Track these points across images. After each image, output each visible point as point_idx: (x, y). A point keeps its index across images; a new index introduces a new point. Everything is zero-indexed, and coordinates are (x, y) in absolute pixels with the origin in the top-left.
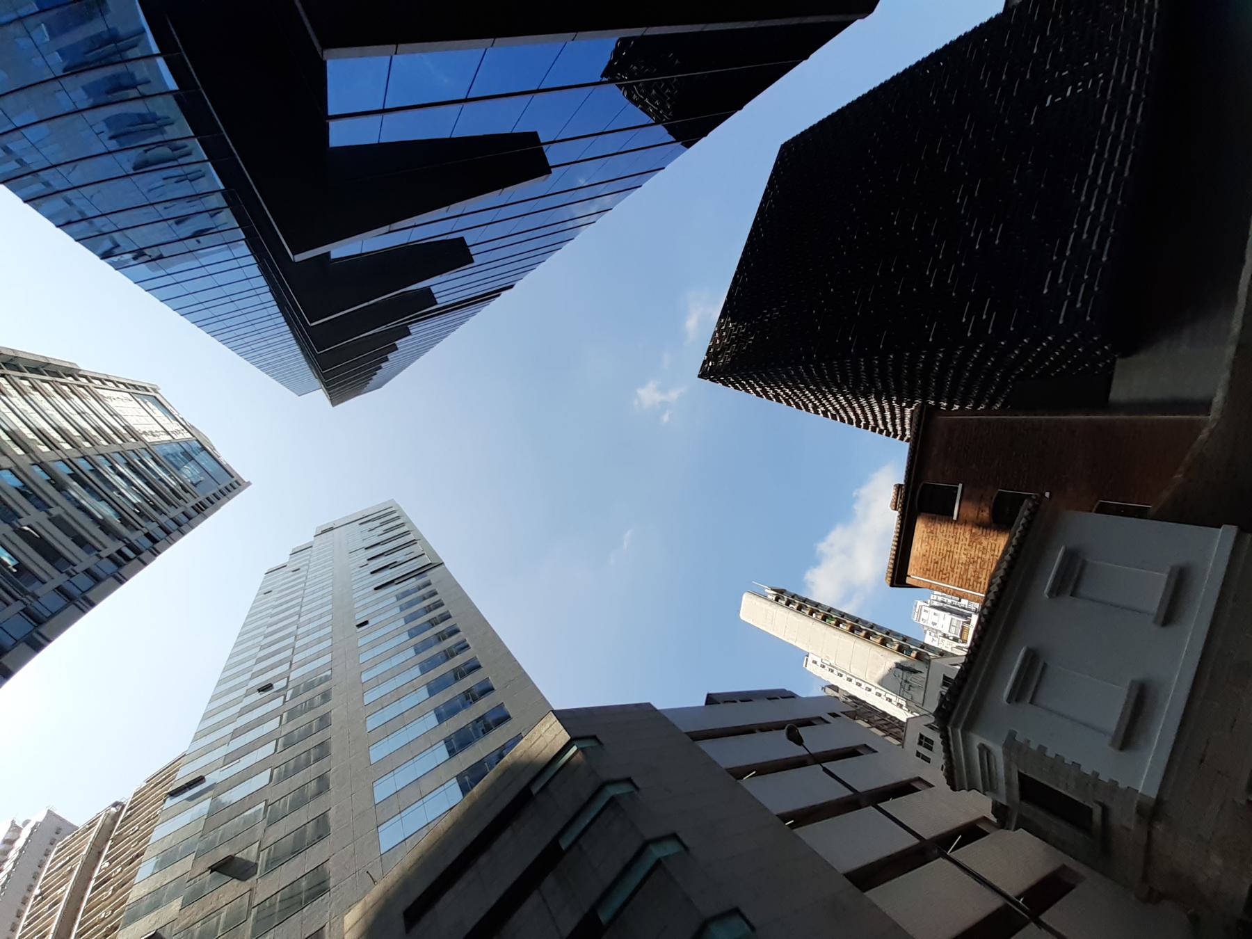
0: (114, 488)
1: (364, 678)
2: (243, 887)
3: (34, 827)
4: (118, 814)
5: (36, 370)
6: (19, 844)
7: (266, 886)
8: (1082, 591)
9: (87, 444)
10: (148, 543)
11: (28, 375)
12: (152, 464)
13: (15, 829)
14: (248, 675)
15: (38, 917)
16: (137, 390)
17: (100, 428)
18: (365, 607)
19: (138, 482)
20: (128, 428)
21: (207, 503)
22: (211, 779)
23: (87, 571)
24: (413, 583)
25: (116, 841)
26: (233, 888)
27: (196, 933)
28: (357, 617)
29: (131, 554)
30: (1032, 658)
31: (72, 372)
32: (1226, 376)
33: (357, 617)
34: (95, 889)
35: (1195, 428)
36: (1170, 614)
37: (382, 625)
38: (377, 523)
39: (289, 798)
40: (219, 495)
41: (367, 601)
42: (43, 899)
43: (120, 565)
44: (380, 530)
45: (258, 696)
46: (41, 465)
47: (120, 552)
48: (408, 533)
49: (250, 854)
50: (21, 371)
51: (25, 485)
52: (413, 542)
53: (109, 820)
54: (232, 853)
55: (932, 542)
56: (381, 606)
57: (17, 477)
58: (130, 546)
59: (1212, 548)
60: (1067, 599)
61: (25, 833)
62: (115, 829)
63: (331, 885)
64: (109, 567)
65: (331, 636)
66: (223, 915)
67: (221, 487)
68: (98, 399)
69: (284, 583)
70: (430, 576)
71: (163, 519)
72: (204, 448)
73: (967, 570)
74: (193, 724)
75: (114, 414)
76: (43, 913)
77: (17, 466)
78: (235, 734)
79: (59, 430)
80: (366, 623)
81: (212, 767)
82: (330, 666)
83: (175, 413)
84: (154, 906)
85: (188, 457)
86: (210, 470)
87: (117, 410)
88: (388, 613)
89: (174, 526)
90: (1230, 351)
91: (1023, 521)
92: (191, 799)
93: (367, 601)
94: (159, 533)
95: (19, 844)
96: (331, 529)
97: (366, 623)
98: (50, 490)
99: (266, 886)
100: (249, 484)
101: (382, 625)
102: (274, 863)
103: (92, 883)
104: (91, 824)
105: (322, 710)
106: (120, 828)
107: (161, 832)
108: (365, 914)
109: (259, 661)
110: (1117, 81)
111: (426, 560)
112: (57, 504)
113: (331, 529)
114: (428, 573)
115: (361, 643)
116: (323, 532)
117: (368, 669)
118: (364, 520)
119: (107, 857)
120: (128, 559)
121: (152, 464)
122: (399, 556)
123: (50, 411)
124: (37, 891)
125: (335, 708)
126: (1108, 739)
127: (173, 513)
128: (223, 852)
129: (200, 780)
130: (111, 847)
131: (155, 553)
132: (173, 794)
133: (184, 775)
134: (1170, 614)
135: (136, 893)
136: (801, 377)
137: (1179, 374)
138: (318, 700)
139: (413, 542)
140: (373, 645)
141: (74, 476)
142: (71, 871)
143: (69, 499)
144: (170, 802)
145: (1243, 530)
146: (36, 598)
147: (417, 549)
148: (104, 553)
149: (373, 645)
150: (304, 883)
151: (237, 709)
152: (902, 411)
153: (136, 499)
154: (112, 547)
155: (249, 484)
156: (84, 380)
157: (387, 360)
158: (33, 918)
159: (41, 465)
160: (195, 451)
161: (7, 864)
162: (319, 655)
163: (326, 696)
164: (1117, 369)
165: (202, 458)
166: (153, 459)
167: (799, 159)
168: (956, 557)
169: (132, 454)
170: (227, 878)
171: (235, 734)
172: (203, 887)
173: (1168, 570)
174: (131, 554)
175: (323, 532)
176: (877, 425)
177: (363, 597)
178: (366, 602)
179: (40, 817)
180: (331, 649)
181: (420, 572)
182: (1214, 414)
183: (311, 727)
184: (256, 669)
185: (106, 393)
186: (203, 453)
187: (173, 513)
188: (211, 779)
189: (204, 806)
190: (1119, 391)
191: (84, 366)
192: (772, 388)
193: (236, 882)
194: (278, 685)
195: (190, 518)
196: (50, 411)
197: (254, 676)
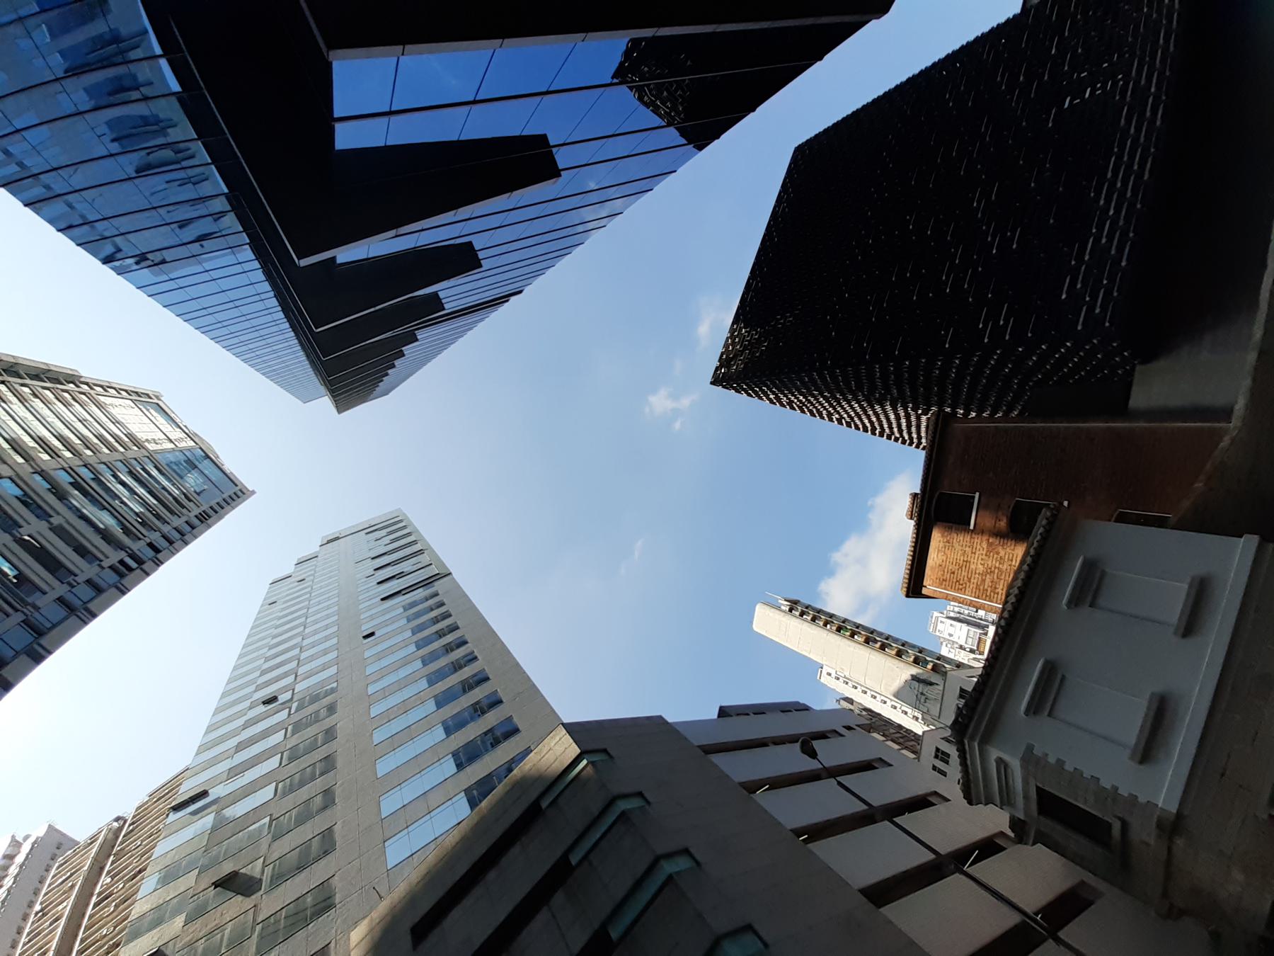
0: (116, 496)
1: (371, 690)
2: (248, 903)
3: (35, 842)
4: (120, 829)
5: (36, 377)
6: (20, 859)
7: (271, 903)
8: (1101, 601)
9: (88, 452)
10: (151, 553)
11: (28, 381)
12: (155, 473)
13: (15, 844)
14: (253, 688)
15: (39, 934)
16: (140, 397)
17: (102, 436)
18: (372, 618)
19: (141, 490)
20: (131, 436)
21: (211, 512)
22: (214, 793)
23: (89, 582)
24: (420, 593)
25: (119, 856)
26: (238, 904)
27: (200, 950)
28: (363, 628)
29: (133, 564)
30: (1050, 670)
31: (73, 379)
32: (1247, 382)
33: (363, 628)
34: (96, 905)
35: (1216, 436)
36: (1190, 625)
37: (388, 636)
38: (384, 532)
39: (294, 812)
40: (223, 504)
41: (373, 611)
42: (44, 915)
43: (122, 576)
44: (387, 540)
45: (262, 708)
46: (42, 473)
47: (122, 562)
48: (415, 542)
49: (255, 869)
50: (21, 378)
51: (26, 494)
52: (420, 552)
53: (110, 835)
54: (236, 869)
55: (948, 552)
56: (387, 617)
57: (18, 485)
58: (133, 556)
59: (1233, 558)
60: (1085, 610)
61: (26, 848)
62: (117, 844)
63: (337, 901)
64: (111, 577)
65: (337, 647)
66: (227, 932)
67: (225, 496)
68: (99, 406)
69: (289, 593)
70: (438, 586)
71: (166, 529)
72: (207, 457)
73: (984, 581)
74: (196, 737)
75: (116, 422)
76: (44, 930)
77: (18, 475)
78: (239, 748)
79: (60, 438)
80: (372, 634)
81: (216, 781)
82: (336, 678)
83: (178, 420)
84: (157, 923)
85: (192, 465)
86: (213, 479)
87: (119, 418)
88: (394, 624)
89: (177, 536)
90: (1252, 357)
91: (1041, 530)
92: (194, 813)
93: (373, 611)
94: (162, 543)
95: (20, 859)
96: (337, 539)
97: (372, 634)
98: (51, 499)
99: (271, 903)
100: (253, 492)
101: (388, 636)
102: (279, 879)
103: (94, 899)
104: (93, 839)
105: (328, 723)
106: (122, 843)
107: (164, 847)
108: (371, 930)
109: (263, 673)
110: (1137, 82)
111: (433, 570)
112: (58, 514)
113: (337, 539)
114: (436, 584)
115: (367, 654)
116: (328, 542)
117: (375, 682)
118: (370, 529)
119: (109, 872)
120: (130, 569)
121: (155, 473)
122: (406, 566)
123: (51, 418)
124: (37, 907)
125: (341, 721)
126: (1128, 752)
127: (177, 522)
128: (227, 868)
129: (204, 794)
130: (113, 863)
131: (158, 563)
132: (176, 808)
133: (187, 789)
134: (1190, 625)
135: (138, 909)
136: (815, 384)
137: (1200, 380)
138: (323, 713)
139: (420, 552)
140: (380, 656)
141: (75, 485)
142: (73, 886)
143: (70, 508)
144: (173, 817)
145: (1265, 540)
146: (37, 608)
147: (424, 559)
148: (106, 564)
149: (380, 656)
150: (309, 899)
151: (241, 722)
152: (918, 418)
153: (138, 508)
154: (114, 556)
155: (253, 492)
156: (85, 387)
157: (394, 366)
158: (34, 935)
159: (42, 473)
160: (198, 459)
161: (7, 879)
162: (324, 667)
163: (331, 709)
164: (1137, 375)
165: (205, 466)
166: (156, 467)
167: (813, 162)
168: (973, 567)
169: (134, 462)
170: (231, 894)
171: (239, 748)
172: (206, 903)
173: (1189, 580)
174: (133, 564)
175: (328, 542)
176: (893, 433)
177: (369, 608)
178: (372, 612)
179: (40, 831)
180: (337, 661)
181: (427, 582)
182: (1236, 422)
183: (316, 740)
184: (260, 681)
185: (108, 400)
186: (207, 462)
187: (177, 522)
188: (214, 793)
189: (208, 820)
190: (1139, 398)
191: (86, 372)
192: (785, 396)
193: (240, 898)
194: (283, 698)
195: (193, 528)
196: (51, 418)
197: (258, 689)
